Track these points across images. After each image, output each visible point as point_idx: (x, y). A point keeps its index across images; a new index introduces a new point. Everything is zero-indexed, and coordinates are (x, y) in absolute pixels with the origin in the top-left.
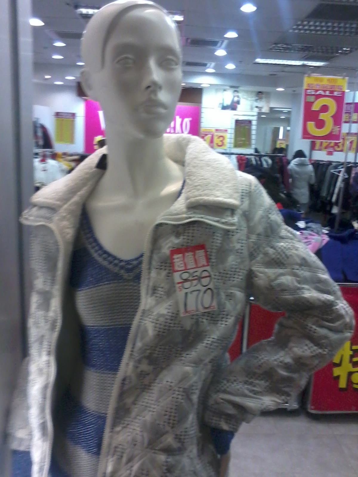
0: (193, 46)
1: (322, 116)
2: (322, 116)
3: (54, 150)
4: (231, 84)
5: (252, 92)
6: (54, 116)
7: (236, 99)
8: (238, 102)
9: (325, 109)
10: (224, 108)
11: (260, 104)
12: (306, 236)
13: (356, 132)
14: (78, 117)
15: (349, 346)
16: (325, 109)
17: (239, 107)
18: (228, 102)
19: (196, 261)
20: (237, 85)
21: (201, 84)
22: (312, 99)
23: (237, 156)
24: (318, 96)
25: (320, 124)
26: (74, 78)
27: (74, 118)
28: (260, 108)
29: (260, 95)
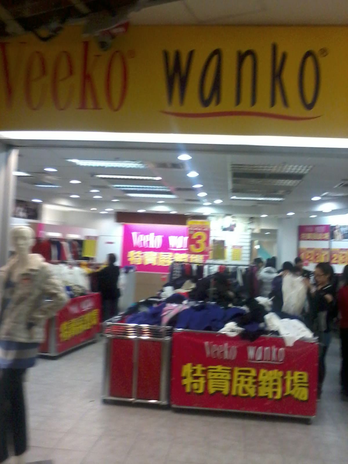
0: (125, 210)
1: (199, 242)
2: (199, 242)
3: (182, 170)
4: (227, 213)
5: (247, 218)
6: (250, 236)
7: (233, 223)
8: (234, 226)
9: (199, 238)
10: (225, 229)
11: (253, 226)
12: (22, 326)
13: (346, 248)
14: (211, 237)
15: (34, 461)
16: (199, 238)
17: (235, 229)
18: (227, 226)
19: (206, 384)
20: (231, 214)
21: (203, 213)
22: (191, 232)
23: (319, 283)
24: (196, 231)
25: (198, 246)
26: (113, 210)
27: (96, 240)
28: (253, 229)
29: (252, 220)
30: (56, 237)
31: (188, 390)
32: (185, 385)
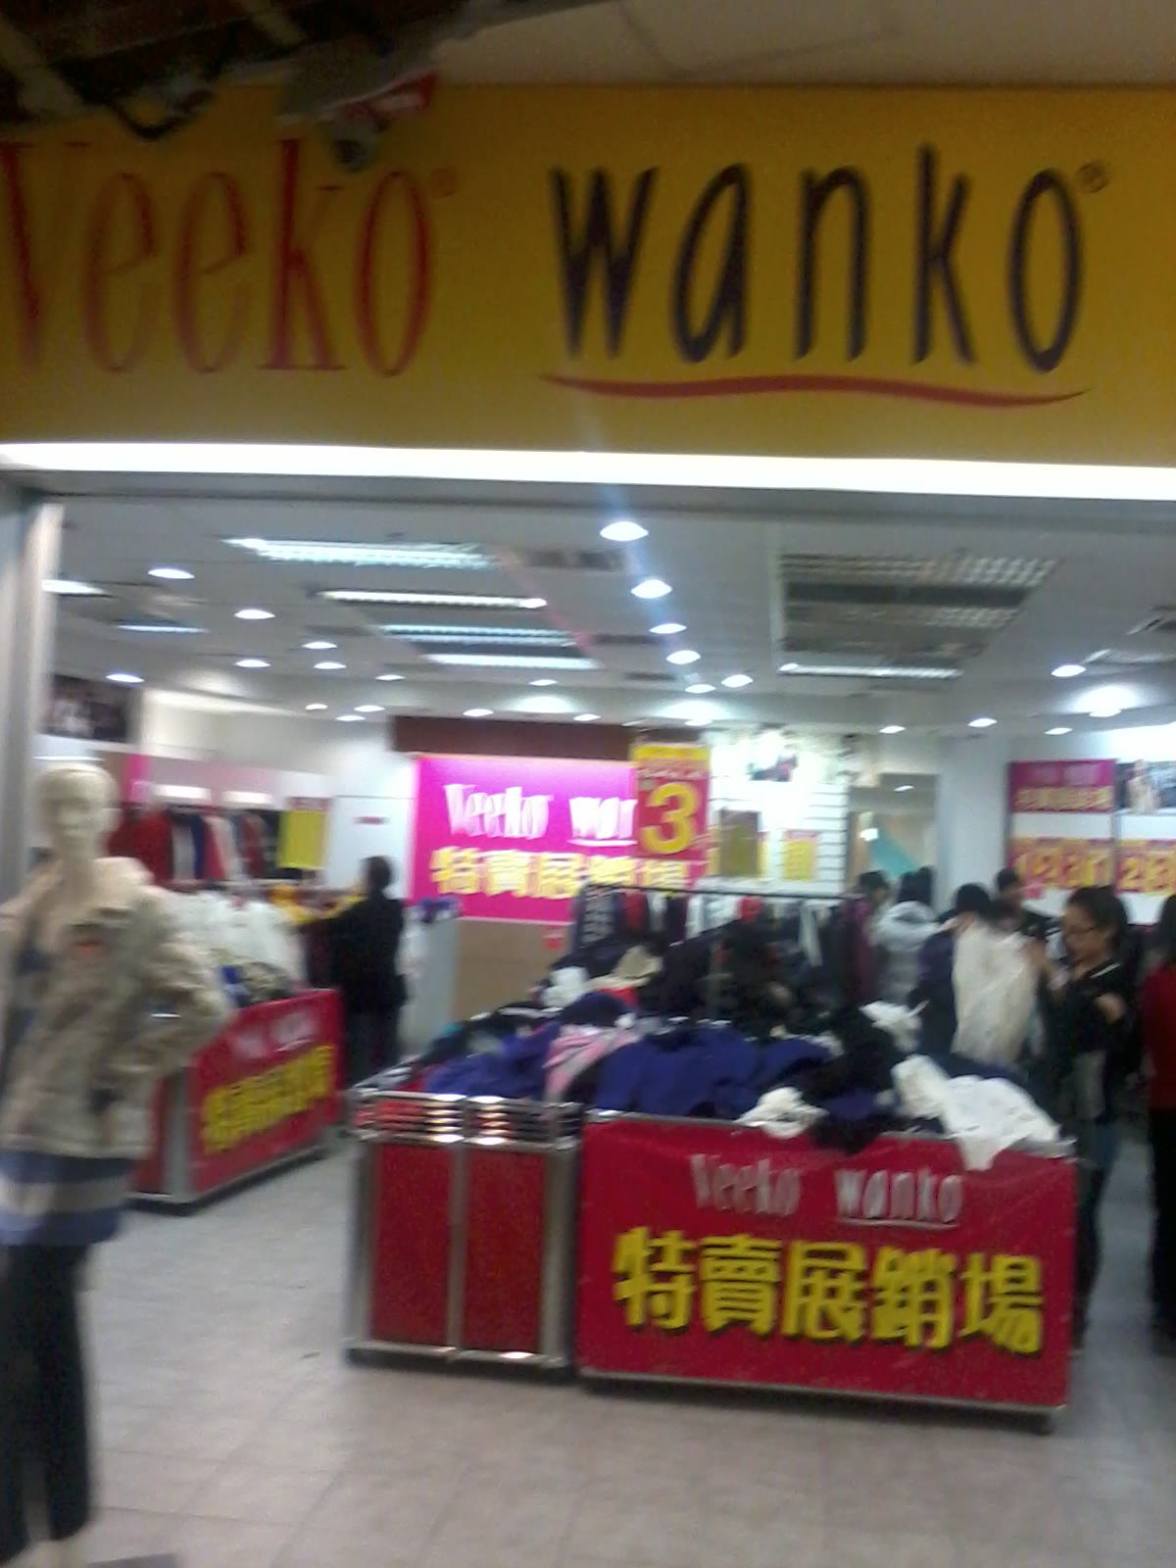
0: (422, 710)
1: (672, 816)
2: (672, 816)
3: (614, 574)
4: (766, 720)
5: (833, 735)
7: (788, 754)
8: (792, 762)
9: (674, 803)
10: (759, 776)
11: (854, 765)
12: (74, 1103)
13: (1171, 836)
14: (712, 803)
16: (674, 803)
17: (795, 773)
18: (767, 763)
20: (780, 722)
21: (686, 720)
22: (647, 786)
23: (1079, 958)
24: (662, 781)
25: (668, 832)
26: (381, 709)
27: (325, 810)
28: (854, 775)
29: (851, 742)
31: (636, 1317)
32: (625, 1302)
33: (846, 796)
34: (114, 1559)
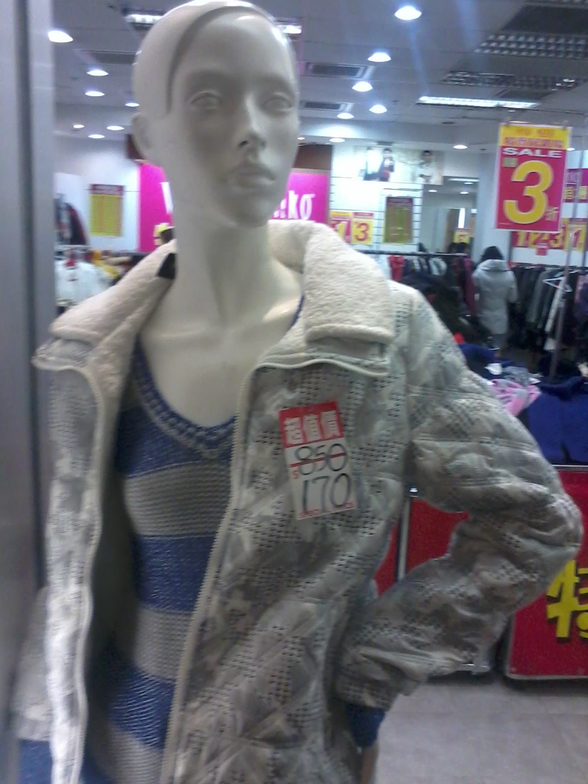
1: (529, 191)
2: (529, 191)
3: (88, 246)
4: (380, 138)
5: (414, 151)
7: (387, 163)
8: (391, 168)
9: (533, 178)
10: (368, 177)
11: (426, 171)
12: (502, 389)
13: (585, 217)
14: (127, 193)
16: (533, 178)
17: (392, 175)
18: (374, 168)
19: (321, 429)
20: (390, 140)
21: (331, 138)
22: (512, 162)
23: (389, 256)
24: (523, 159)
25: (526, 204)
26: (121, 128)
27: (121, 194)
28: (426, 178)
29: (426, 156)
30: (218, 3)
31: (563, 631)
32: (555, 620)
33: (89, 191)
34: (574, 569)
